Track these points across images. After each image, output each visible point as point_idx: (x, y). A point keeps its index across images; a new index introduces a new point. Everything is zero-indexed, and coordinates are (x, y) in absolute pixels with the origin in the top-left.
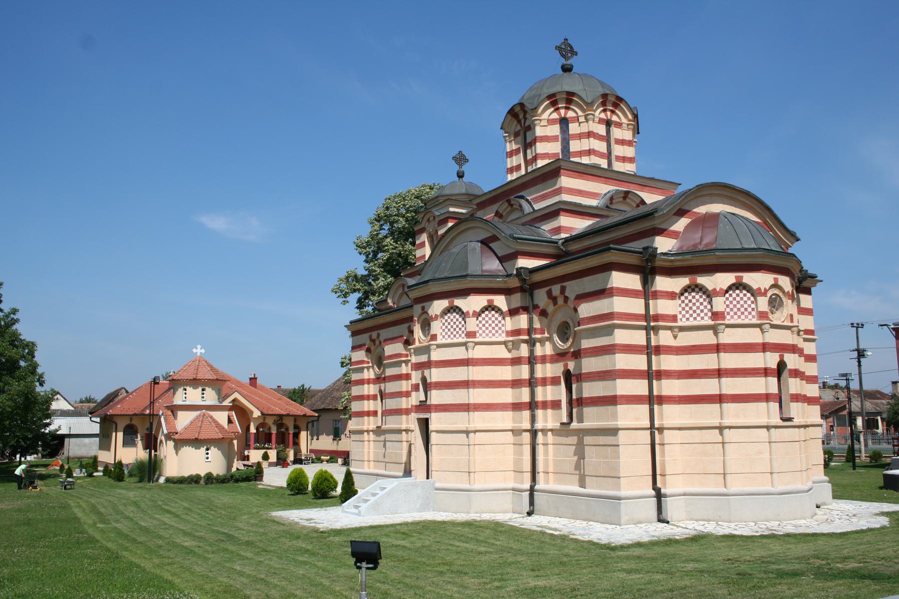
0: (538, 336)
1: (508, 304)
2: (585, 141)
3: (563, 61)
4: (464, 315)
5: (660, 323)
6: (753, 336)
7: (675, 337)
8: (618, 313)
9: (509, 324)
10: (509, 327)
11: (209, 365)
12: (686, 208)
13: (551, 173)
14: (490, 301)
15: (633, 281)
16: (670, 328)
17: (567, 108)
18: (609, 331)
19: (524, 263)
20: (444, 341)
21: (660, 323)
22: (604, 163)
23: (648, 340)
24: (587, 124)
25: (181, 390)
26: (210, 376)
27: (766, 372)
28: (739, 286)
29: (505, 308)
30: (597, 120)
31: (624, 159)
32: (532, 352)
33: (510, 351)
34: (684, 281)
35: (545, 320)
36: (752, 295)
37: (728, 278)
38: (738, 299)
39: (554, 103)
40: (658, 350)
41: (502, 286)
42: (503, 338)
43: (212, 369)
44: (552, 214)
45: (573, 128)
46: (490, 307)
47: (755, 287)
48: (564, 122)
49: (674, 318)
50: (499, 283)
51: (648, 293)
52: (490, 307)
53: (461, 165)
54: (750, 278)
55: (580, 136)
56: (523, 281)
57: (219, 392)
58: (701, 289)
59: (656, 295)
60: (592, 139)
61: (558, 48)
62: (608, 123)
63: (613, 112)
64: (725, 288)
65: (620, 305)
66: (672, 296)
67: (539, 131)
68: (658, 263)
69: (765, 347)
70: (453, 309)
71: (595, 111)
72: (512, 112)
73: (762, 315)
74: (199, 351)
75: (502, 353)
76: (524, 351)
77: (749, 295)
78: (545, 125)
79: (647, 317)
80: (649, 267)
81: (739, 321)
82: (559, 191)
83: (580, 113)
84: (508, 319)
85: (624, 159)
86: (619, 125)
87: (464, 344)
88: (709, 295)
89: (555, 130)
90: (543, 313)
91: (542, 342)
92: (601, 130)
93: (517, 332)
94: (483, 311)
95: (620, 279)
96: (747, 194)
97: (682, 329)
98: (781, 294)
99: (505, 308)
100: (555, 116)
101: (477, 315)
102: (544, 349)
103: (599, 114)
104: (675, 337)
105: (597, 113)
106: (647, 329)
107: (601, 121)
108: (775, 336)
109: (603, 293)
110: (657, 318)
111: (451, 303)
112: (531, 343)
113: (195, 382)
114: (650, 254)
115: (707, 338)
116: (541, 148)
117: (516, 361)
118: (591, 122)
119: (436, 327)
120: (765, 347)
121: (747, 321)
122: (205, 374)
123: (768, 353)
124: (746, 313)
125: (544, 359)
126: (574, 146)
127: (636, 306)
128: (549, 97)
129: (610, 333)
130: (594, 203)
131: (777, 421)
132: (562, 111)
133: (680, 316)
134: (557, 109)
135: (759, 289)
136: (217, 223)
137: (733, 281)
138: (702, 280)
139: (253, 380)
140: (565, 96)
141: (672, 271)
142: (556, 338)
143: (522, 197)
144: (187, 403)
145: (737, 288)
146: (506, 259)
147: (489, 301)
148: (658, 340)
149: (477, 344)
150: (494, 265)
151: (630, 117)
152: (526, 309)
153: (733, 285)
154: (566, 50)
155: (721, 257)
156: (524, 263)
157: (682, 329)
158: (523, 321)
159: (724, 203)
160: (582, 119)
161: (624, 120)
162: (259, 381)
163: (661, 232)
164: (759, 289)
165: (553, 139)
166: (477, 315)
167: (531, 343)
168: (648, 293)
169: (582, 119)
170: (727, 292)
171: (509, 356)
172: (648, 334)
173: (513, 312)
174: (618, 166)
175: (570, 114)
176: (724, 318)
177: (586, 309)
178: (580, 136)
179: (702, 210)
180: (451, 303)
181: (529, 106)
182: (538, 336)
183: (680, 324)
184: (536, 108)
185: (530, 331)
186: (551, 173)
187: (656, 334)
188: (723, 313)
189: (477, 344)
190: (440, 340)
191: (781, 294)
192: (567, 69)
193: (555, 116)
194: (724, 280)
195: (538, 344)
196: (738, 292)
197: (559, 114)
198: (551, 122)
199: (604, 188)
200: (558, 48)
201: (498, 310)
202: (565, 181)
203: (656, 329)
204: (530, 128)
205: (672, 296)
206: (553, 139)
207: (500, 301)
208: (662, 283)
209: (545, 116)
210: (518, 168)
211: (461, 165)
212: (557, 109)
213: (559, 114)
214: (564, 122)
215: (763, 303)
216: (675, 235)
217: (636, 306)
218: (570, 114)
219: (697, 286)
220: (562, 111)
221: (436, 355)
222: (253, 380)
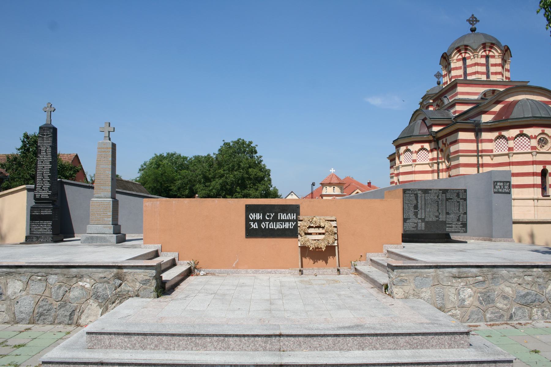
0: (440, 161)
1: (430, 146)
2: (473, 67)
3: (471, 26)
4: (412, 153)
5: (483, 154)
6: (529, 158)
7: (492, 159)
8: (461, 150)
9: (431, 155)
10: (431, 157)
11: (336, 177)
12: (501, 100)
13: (453, 86)
14: (422, 146)
15: (471, 136)
16: (489, 155)
17: (466, 53)
18: (457, 158)
19: (435, 129)
20: (405, 164)
21: (483, 154)
22: (484, 78)
23: (478, 161)
24: (476, 59)
25: (325, 188)
26: (336, 181)
27: (534, 174)
28: (522, 135)
29: (429, 149)
30: (480, 56)
31: (496, 73)
32: (438, 167)
33: (431, 167)
34: (496, 134)
35: (443, 154)
36: (529, 139)
37: (516, 132)
38: (521, 141)
39: (459, 51)
40: (483, 165)
41: (427, 139)
42: (428, 162)
43: (338, 178)
44: (453, 105)
45: (469, 62)
46: (423, 149)
47: (529, 135)
48: (464, 59)
49: (492, 151)
50: (425, 138)
51: (478, 140)
52: (423, 149)
53: (439, 78)
54: (526, 131)
55: (471, 66)
56: (434, 137)
57: (341, 189)
58: (503, 137)
59: (483, 141)
60: (476, 67)
61: (468, 21)
62: (487, 57)
63: (490, 51)
64: (514, 136)
65: (462, 146)
66: (490, 141)
67: (453, 65)
68: (482, 127)
69: (534, 163)
70: (408, 150)
71: (478, 52)
72: (443, 56)
73: (533, 148)
74: (332, 171)
75: (428, 168)
76: (435, 166)
77: (527, 139)
78: (456, 62)
79: (478, 151)
80: (478, 129)
81: (522, 151)
82: (456, 94)
83: (471, 54)
84: (430, 153)
85: (496, 73)
86: (493, 57)
87: (411, 165)
88: (507, 139)
89: (460, 64)
90: (442, 151)
91: (442, 163)
92: (483, 61)
93: (433, 159)
94: (420, 150)
95: (462, 135)
96: (541, 88)
97: (495, 156)
98: (547, 137)
99: (429, 149)
100: (460, 57)
101: (417, 152)
102: (443, 166)
103: (481, 53)
104: (492, 159)
105: (480, 53)
106: (478, 156)
107: (482, 56)
108: (540, 158)
109: (456, 142)
110: (482, 151)
111: (407, 147)
112: (438, 163)
113: (330, 184)
114: (478, 124)
115: (505, 159)
116: (453, 73)
117: (433, 172)
118: (476, 58)
119: (402, 157)
120: (534, 163)
121: (526, 151)
122: (335, 181)
123: (535, 166)
124: (525, 147)
125: (442, 171)
126: (469, 70)
127: (472, 146)
128: (456, 49)
129: (458, 159)
130: (476, 97)
131: (540, 196)
132: (463, 54)
133: (494, 150)
134: (461, 54)
135: (532, 136)
136: (376, 101)
137: (519, 133)
138: (504, 133)
139: (369, 184)
140: (464, 47)
141: (491, 130)
142: (446, 161)
143: (446, 97)
144: (327, 193)
145: (521, 136)
146: (429, 127)
147: (422, 146)
148: (482, 161)
149: (416, 165)
150: (425, 130)
151: (499, 52)
152: (435, 149)
153: (519, 134)
154: (473, 20)
155: (510, 122)
156: (435, 129)
157: (495, 156)
158: (435, 154)
159: (526, 94)
160: (472, 57)
161: (496, 54)
162: (372, 184)
163: (485, 112)
164: (532, 136)
165: (459, 68)
166: (417, 152)
167: (438, 163)
168: (478, 140)
169: (472, 57)
170: (516, 138)
171: (430, 169)
172: (478, 159)
173: (432, 151)
174: (493, 78)
175: (467, 55)
176: (513, 150)
177: (453, 149)
178: (471, 66)
179: (511, 99)
180: (407, 147)
181: (448, 54)
182: (440, 161)
183: (494, 153)
184: (451, 55)
185: (438, 158)
186: (453, 86)
187: (482, 158)
188: (513, 148)
189: (416, 165)
190: (403, 164)
191: (547, 137)
192: (473, 30)
193: (460, 57)
194: (514, 132)
195: (440, 164)
196: (521, 137)
197: (462, 56)
198: (458, 60)
199: (482, 90)
200: (468, 21)
201: (426, 150)
202: (460, 89)
203: (482, 156)
204: (449, 64)
205: (490, 141)
206: (459, 68)
207: (427, 146)
208: (485, 135)
209: (455, 58)
210: (447, 82)
211: (439, 78)
212: (461, 54)
213: (462, 56)
214: (464, 59)
215: (534, 142)
216: (493, 113)
217: (472, 146)
218: (467, 55)
219: (502, 136)
220: (463, 54)
221: (402, 170)
222: (369, 184)
